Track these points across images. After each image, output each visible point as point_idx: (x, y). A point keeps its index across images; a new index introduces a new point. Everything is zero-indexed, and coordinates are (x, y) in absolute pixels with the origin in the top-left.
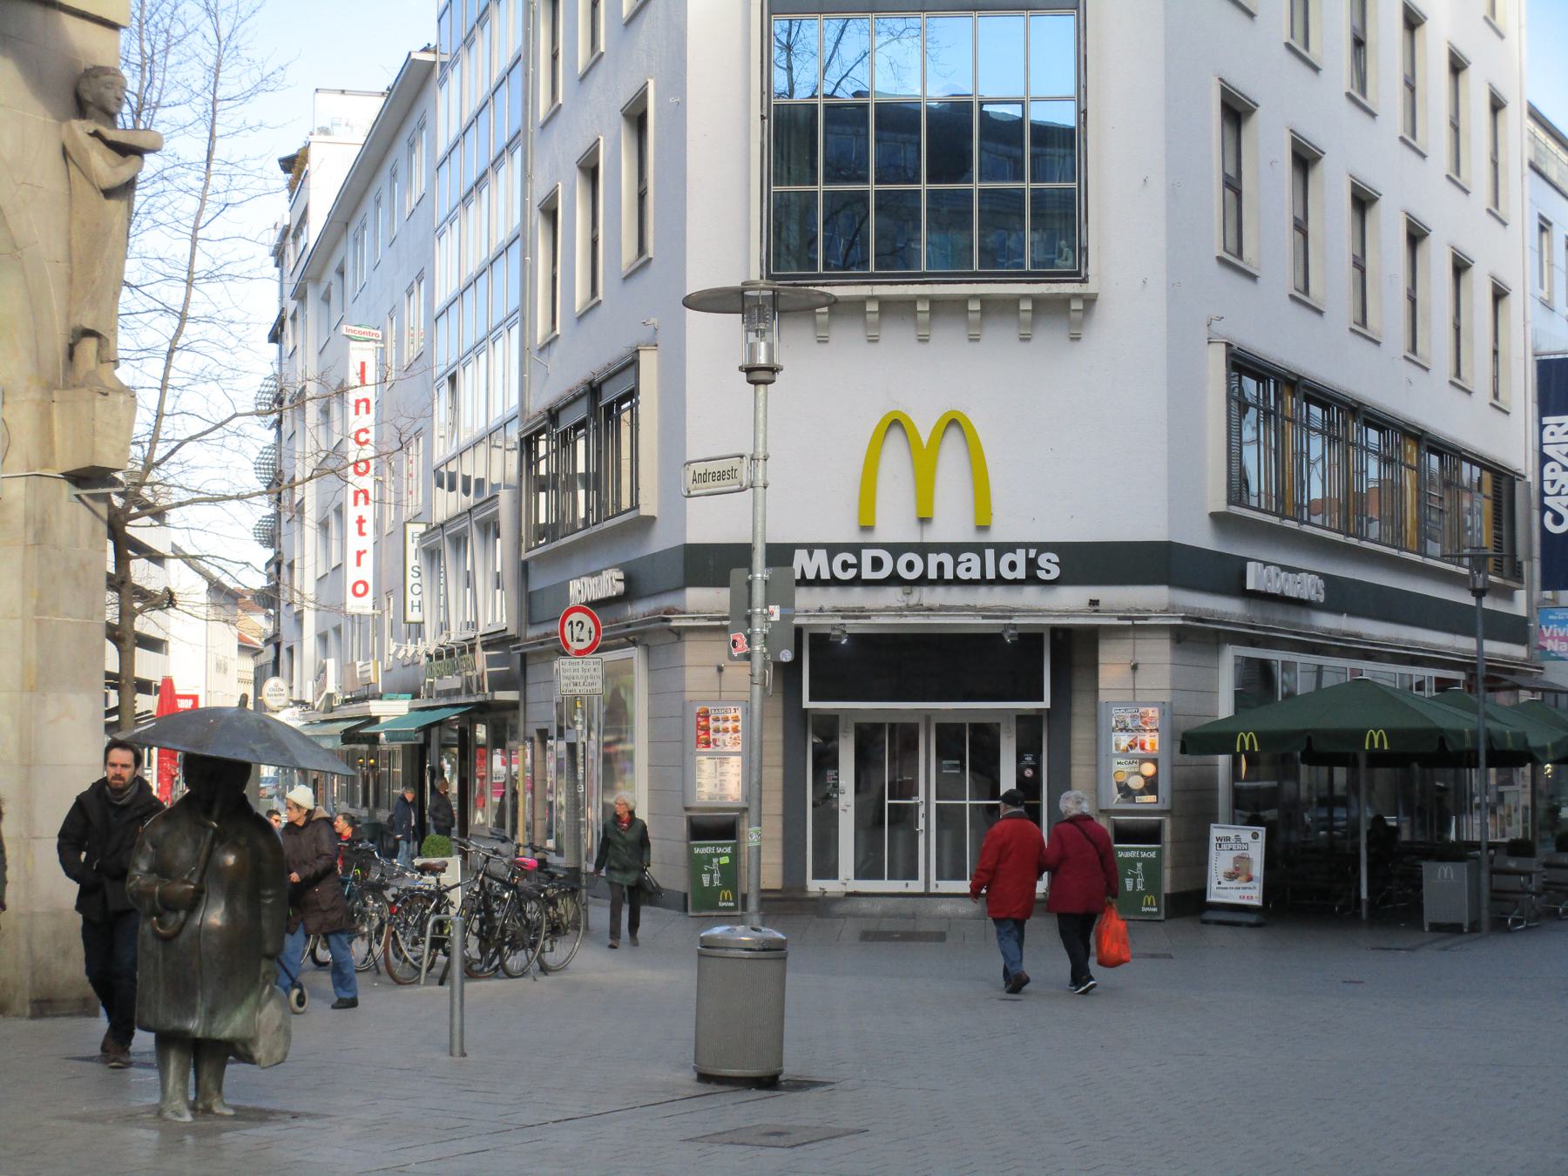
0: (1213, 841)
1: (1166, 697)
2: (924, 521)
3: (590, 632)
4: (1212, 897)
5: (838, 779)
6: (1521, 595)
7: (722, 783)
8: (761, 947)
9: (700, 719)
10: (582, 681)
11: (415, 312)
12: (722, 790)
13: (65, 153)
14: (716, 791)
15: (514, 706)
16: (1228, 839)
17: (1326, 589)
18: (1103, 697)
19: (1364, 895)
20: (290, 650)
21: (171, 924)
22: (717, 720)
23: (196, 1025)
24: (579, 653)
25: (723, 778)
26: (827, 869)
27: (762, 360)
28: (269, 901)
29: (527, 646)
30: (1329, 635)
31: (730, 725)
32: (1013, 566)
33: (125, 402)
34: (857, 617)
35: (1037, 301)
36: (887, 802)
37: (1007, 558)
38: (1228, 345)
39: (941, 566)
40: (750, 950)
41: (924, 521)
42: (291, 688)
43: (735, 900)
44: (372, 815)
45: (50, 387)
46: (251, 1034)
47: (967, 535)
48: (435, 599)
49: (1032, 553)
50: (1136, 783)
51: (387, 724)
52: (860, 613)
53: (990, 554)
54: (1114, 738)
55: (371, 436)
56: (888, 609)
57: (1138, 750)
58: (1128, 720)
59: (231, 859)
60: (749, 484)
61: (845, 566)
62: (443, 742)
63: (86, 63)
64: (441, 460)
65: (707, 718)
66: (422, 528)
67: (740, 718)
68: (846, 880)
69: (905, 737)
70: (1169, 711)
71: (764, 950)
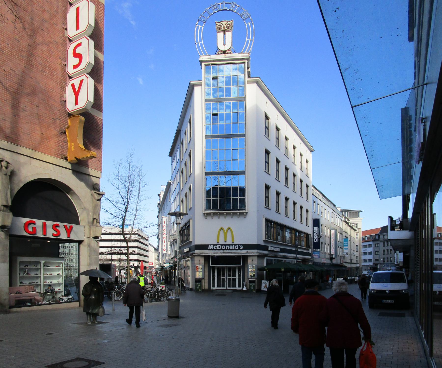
0: (262, 283)
1: (256, 264)
2: (225, 241)
6: (310, 250)
13: (92, 195)
16: (264, 282)
17: (280, 250)
18: (248, 264)
19: (283, 289)
26: (214, 286)
27: (178, 222)
30: (280, 256)
31: (200, 268)
32: (237, 247)
35: (240, 213)
38: (266, 218)
39: (227, 247)
41: (225, 241)
45: (90, 226)
49: (239, 245)
50: (252, 275)
52: (217, 253)
53: (234, 246)
55: (166, 230)
56: (221, 253)
59: (95, 289)
61: (215, 247)
63: (95, 183)
65: (198, 267)
69: (223, 269)
70: (257, 266)
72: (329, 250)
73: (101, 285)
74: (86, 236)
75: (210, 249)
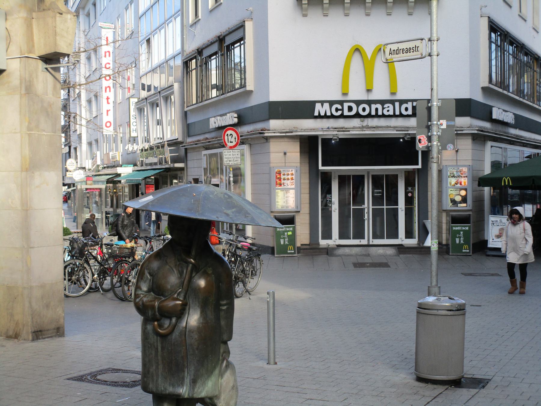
2: (369, 91)
3: (235, 139)
4: (490, 245)
5: (331, 198)
7: (287, 202)
8: (456, 309)
9: (277, 175)
10: (232, 159)
11: (130, 17)
12: (287, 204)
14: (284, 204)
15: (182, 169)
16: (497, 221)
20: (75, 149)
21: (166, 326)
22: (284, 175)
23: (184, 390)
24: (231, 147)
25: (287, 199)
26: (327, 235)
28: (224, 308)
29: (188, 145)
30: (517, 137)
32: (406, 109)
33: (70, 19)
34: (344, 131)
36: (352, 207)
37: (404, 106)
39: (377, 110)
40: (451, 310)
41: (369, 91)
42: (77, 162)
43: (294, 250)
44: (115, 211)
46: (217, 393)
47: (386, 96)
48: (143, 127)
50: (458, 199)
51: (125, 177)
53: (397, 104)
54: (449, 180)
55: (111, 66)
57: (459, 185)
58: (455, 173)
59: (202, 283)
60: (427, 54)
61: (337, 110)
62: (146, 183)
64: (143, 73)
65: (280, 174)
66: (136, 100)
67: (294, 174)
68: (335, 240)
69: (359, 180)
71: (458, 310)
72: (319, 132)
73: (223, 261)
74: (14, 51)
75: (320, 117)
